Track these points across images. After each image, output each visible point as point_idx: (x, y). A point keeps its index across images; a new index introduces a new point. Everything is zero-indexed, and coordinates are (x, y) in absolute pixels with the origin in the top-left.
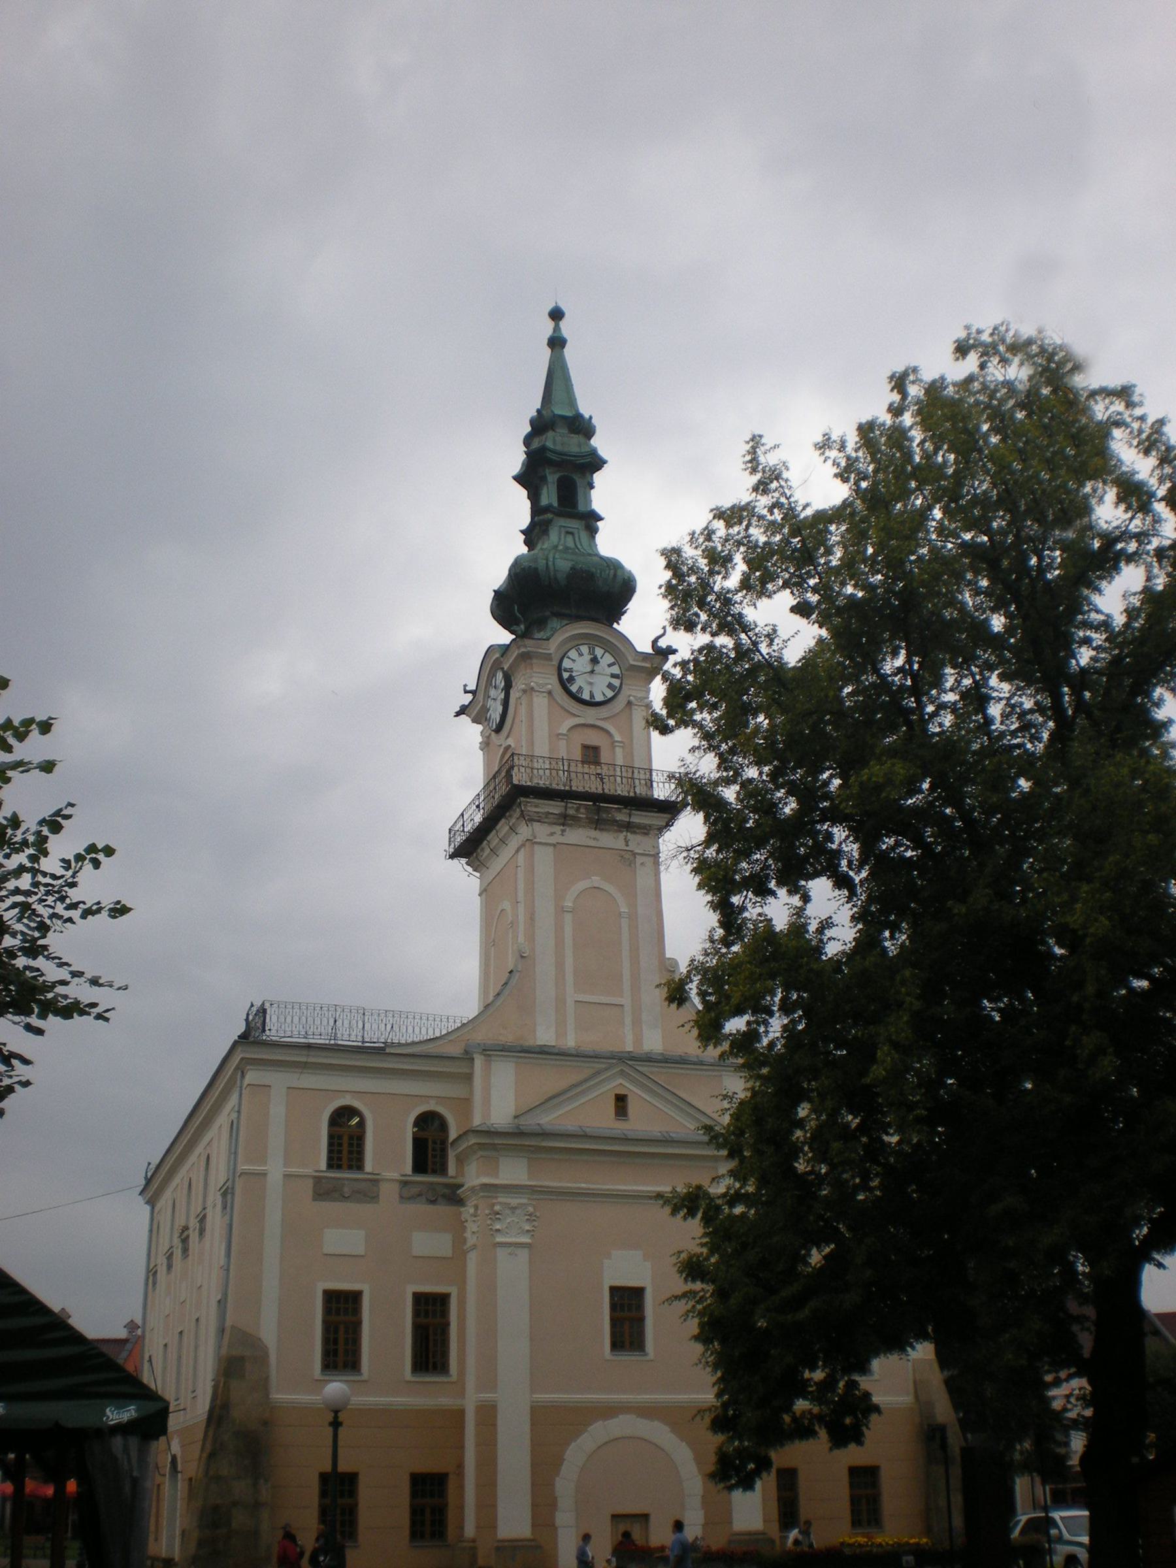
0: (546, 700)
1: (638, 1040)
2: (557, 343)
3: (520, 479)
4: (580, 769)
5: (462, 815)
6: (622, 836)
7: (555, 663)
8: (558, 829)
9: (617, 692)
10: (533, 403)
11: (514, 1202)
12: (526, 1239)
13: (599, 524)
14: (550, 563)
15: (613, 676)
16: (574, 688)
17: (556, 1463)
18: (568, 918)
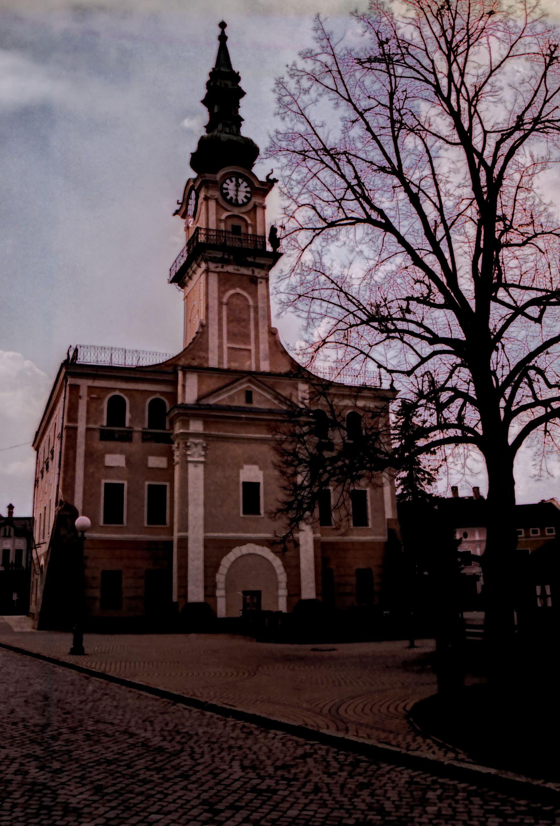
1: (258, 366)
2: (223, 38)
3: (204, 102)
4: (231, 236)
6: (251, 269)
7: (219, 185)
9: (249, 199)
11: (197, 441)
12: (202, 459)
13: (242, 122)
15: (247, 192)
17: (216, 567)
18: (224, 308)
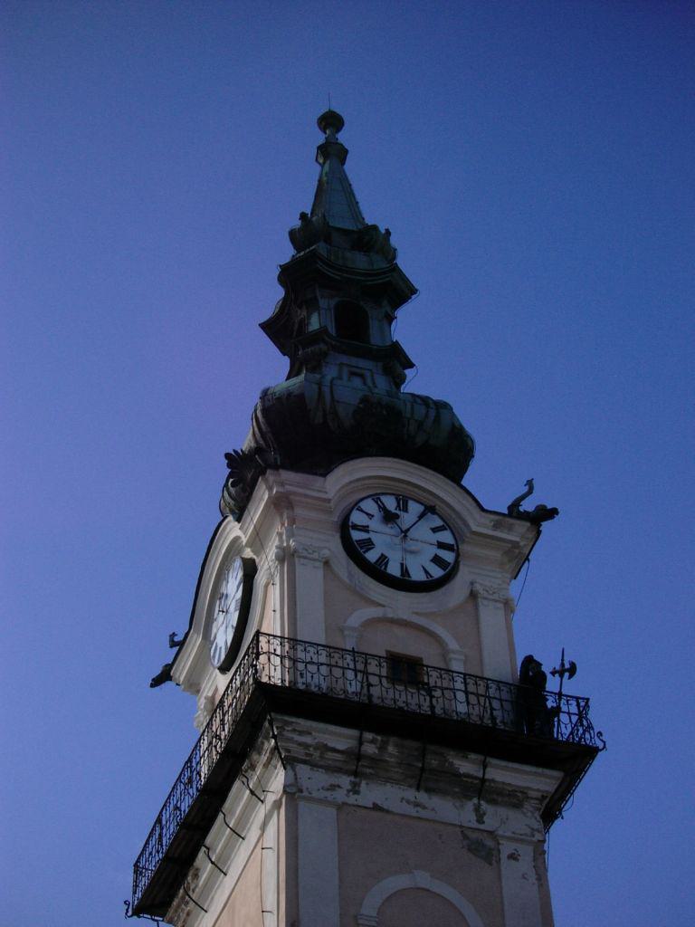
0: (320, 573)
2: (332, 153)
5: (159, 820)
6: (470, 805)
7: (336, 518)
8: (345, 781)
9: (451, 573)
10: (296, 196)
14: (326, 390)
15: (441, 545)
16: (372, 556)
